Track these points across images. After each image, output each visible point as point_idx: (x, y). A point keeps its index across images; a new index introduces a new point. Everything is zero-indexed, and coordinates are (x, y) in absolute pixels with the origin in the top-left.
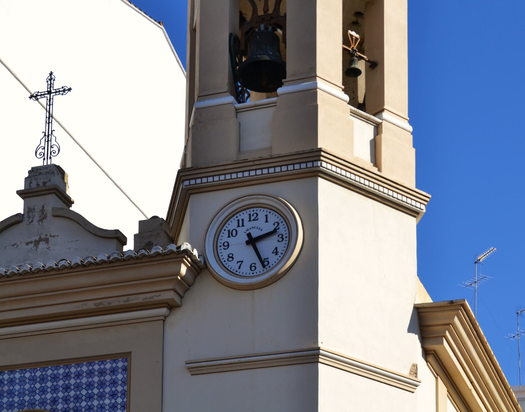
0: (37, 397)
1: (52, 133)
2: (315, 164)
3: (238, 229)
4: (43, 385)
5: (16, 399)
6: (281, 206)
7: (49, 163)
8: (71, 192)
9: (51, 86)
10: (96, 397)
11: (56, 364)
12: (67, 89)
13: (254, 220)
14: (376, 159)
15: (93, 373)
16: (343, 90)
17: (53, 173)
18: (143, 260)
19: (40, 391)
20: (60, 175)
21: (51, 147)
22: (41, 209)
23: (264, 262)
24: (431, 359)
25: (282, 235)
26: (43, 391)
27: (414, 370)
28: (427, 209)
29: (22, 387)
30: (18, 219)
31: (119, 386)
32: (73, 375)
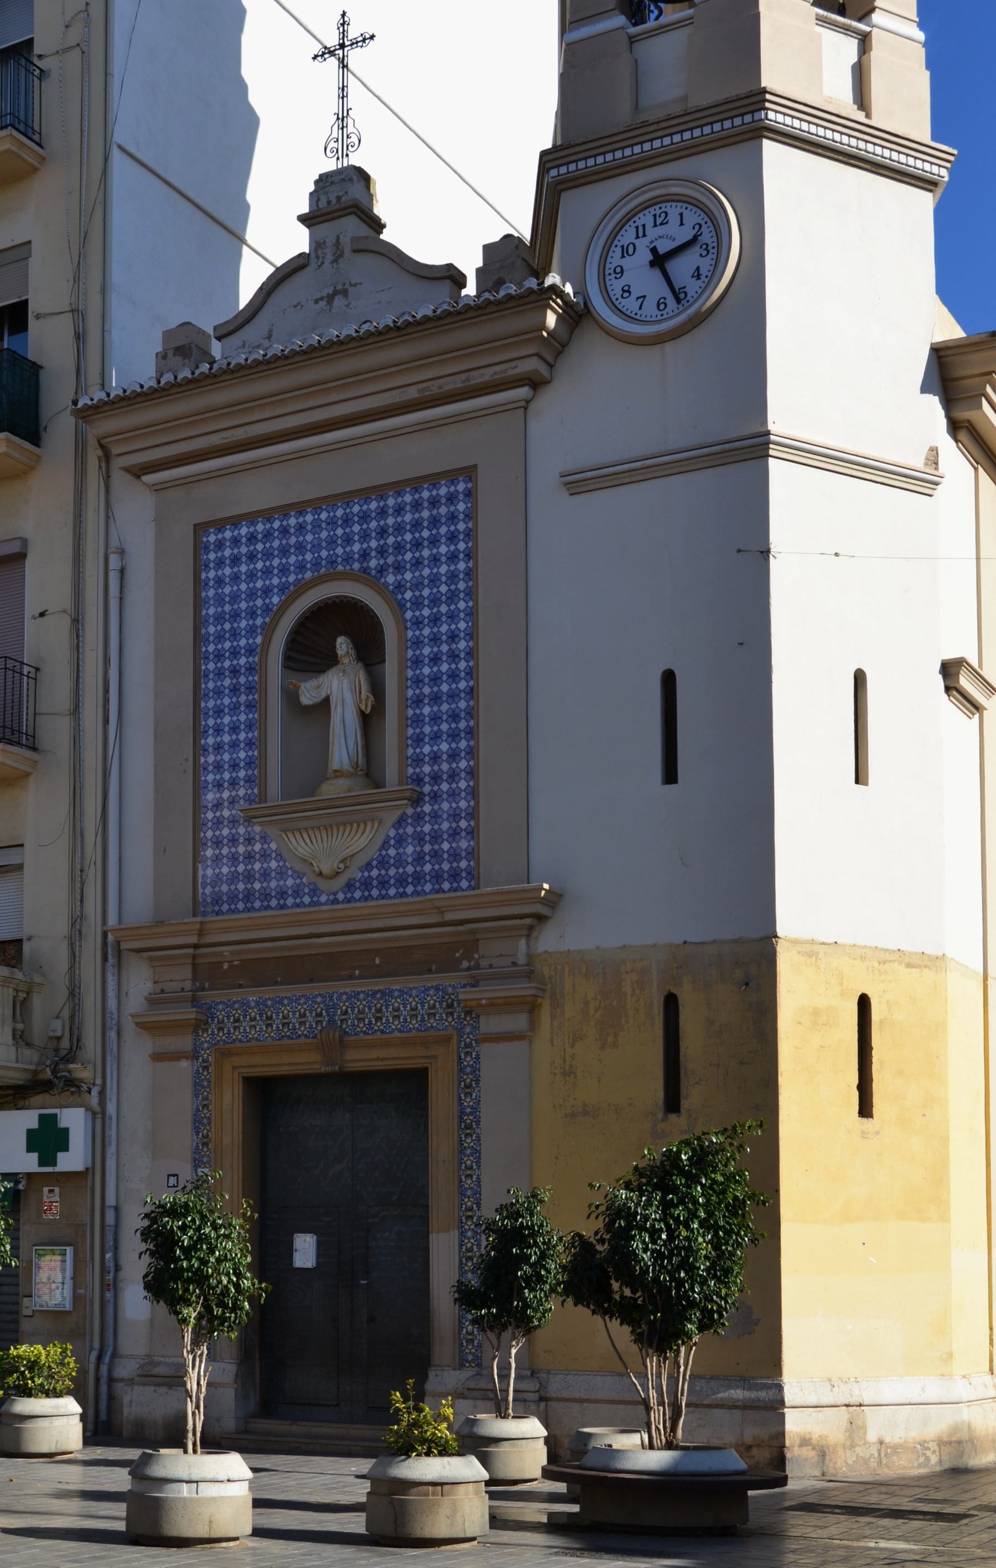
0: (339, 551)
1: (348, 114)
2: (756, 115)
3: (637, 242)
4: (348, 530)
5: (309, 556)
6: (704, 194)
7: (345, 164)
8: (379, 210)
9: (344, 34)
10: (426, 543)
11: (365, 494)
12: (368, 36)
13: (661, 224)
14: (862, 98)
15: (421, 505)
17: (351, 179)
18: (488, 310)
19: (344, 541)
20: (363, 183)
21: (348, 137)
22: (334, 242)
23: (678, 295)
24: (963, 435)
25: (707, 245)
26: (348, 540)
27: (933, 458)
28: (950, 176)
29: (316, 536)
30: (301, 261)
31: (461, 522)
32: (391, 511)
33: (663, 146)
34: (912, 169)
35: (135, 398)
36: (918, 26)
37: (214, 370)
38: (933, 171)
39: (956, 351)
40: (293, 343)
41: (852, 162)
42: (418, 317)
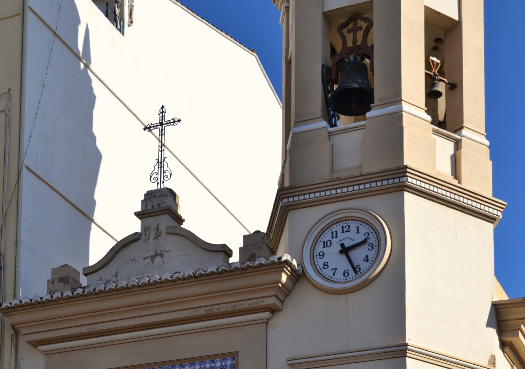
1: (164, 160)
2: (401, 180)
3: (332, 240)
7: (162, 187)
8: (181, 212)
9: (162, 118)
12: (176, 120)
13: (346, 232)
14: (456, 172)
16: (426, 111)
20: (172, 197)
21: (164, 172)
22: (156, 228)
23: (356, 269)
24: (507, 349)
25: (372, 244)
27: (493, 361)
30: (136, 237)
33: (348, 191)
34: (466, 205)
35: (37, 304)
36: (486, 137)
37: (85, 293)
38: (486, 210)
39: (505, 306)
40: (134, 281)
41: (451, 206)
42: (208, 272)
